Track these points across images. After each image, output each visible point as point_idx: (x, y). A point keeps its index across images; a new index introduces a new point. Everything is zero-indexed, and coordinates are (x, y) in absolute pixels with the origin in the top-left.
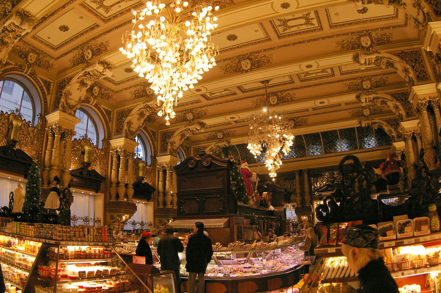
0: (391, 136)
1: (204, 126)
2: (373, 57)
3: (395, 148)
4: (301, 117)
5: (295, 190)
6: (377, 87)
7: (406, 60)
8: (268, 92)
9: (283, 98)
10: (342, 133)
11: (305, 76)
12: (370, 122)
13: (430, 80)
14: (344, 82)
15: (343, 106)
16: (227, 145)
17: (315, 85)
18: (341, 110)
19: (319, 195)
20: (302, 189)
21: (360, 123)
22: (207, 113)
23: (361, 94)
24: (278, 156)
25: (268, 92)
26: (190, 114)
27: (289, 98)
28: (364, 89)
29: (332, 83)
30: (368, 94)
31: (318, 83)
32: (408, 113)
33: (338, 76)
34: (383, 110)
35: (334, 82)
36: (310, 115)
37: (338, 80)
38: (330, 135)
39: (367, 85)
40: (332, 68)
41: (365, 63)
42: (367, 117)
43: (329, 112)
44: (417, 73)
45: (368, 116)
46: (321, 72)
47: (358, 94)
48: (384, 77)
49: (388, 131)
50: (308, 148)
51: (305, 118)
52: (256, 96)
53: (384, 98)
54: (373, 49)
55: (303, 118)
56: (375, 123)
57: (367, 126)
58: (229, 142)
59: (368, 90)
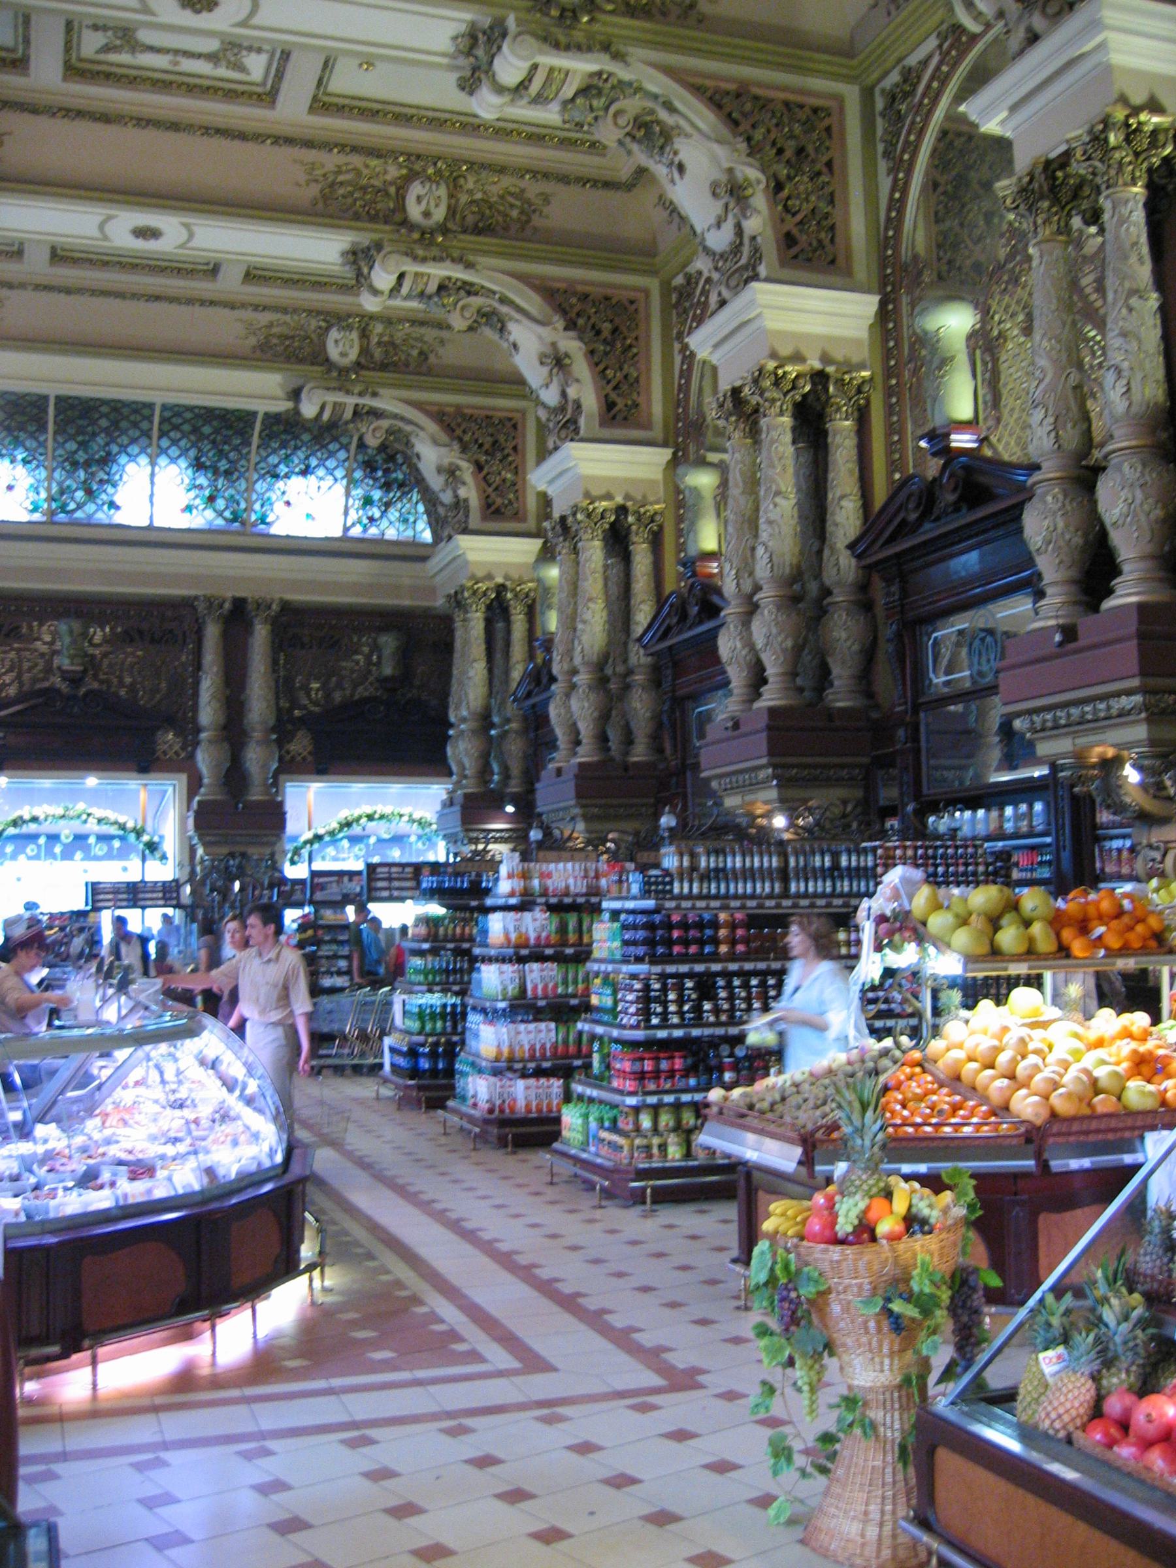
1: (954, 197)
2: (581, 66)
6: (477, 231)
7: (749, 139)
11: (107, 49)
12: (351, 401)
13: (848, 272)
14: (312, 155)
15: (230, 283)
21: (295, 395)
23: (379, 246)
28: (405, 222)
29: (242, 136)
31: (161, 114)
32: (610, 405)
33: (292, 109)
34: (432, 359)
35: (258, 137)
38: (104, 423)
39: (424, 203)
40: (286, 55)
41: (523, 85)
42: (343, 372)
43: (135, 296)
44: (790, 223)
46: (213, 58)
47: (364, 238)
48: (533, 189)
53: (504, 300)
54: (596, 27)
56: (376, 414)
57: (326, 416)
59: (426, 236)
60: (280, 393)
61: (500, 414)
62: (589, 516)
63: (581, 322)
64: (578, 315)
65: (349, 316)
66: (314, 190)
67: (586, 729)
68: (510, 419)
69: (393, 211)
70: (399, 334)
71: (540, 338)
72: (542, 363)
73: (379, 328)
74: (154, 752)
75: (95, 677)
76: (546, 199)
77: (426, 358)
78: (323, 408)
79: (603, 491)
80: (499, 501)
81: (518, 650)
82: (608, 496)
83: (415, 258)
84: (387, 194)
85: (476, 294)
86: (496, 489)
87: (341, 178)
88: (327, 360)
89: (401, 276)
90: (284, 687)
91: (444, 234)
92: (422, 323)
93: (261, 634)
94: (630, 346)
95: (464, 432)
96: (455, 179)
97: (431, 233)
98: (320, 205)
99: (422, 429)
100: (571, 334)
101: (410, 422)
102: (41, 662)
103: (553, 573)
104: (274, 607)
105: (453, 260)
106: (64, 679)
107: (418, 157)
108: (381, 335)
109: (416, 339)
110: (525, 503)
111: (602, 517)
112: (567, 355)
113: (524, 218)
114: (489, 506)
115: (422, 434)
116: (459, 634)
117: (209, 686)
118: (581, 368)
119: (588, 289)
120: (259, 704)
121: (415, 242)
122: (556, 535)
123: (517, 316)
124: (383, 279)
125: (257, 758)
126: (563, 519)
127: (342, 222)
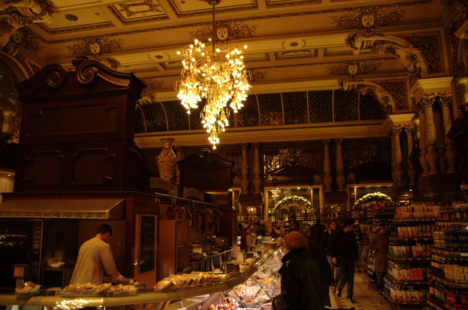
0: (386, 106)
3: (391, 122)
4: (257, 68)
5: (240, 170)
6: (383, 25)
8: (216, 19)
9: (237, 32)
10: (312, 97)
12: (356, 83)
16: (150, 101)
17: (288, 15)
18: (317, 64)
19: (273, 180)
20: (250, 169)
21: (341, 84)
22: (121, 46)
23: (355, 35)
24: (223, 112)
25: (216, 19)
26: (96, 45)
27: (246, 32)
28: (362, 27)
30: (367, 35)
34: (378, 69)
36: (271, 67)
37: (326, 9)
39: (367, 21)
42: (353, 76)
43: (298, 65)
45: (355, 75)
47: (351, 34)
49: (383, 98)
50: (262, 114)
51: (263, 71)
52: (196, 24)
53: (394, 43)
55: (259, 70)
56: (364, 86)
57: (350, 89)
58: (152, 98)
60: (338, 84)
61: (399, 81)
62: (427, 101)
63: (419, 45)
64: (417, 43)
65: (353, 61)
66: (336, 24)
67: (432, 165)
68: (402, 82)
69: (358, 25)
70: (368, 64)
71: (406, 52)
72: (407, 59)
73: (362, 63)
74: (313, 180)
75: (298, 162)
76: (404, 12)
77: (376, 69)
78: (349, 86)
79: (430, 93)
80: (401, 105)
81: (410, 146)
82: (433, 94)
83: (366, 36)
84: (356, 20)
85: (385, 43)
86: (399, 101)
87: (343, 19)
88: (349, 74)
89: (363, 42)
90: (346, 162)
91: (374, 28)
92: (373, 60)
93: (339, 147)
94: (435, 49)
95: (389, 87)
96: (375, 12)
97: (370, 29)
98: (338, 28)
99: (377, 88)
100: (416, 49)
101: (373, 87)
102: (285, 159)
103: (418, 121)
104: (329, 141)
105: (377, 35)
106: (290, 163)
107: (363, 7)
108: (363, 65)
109: (372, 64)
110: (408, 104)
111: (431, 100)
112: (415, 55)
113: (397, 19)
114: (398, 106)
115: (377, 89)
116: (393, 142)
117: (326, 162)
118: (420, 58)
119: (419, 35)
120: (340, 166)
121: (366, 32)
122: (418, 109)
123: (398, 47)
124: (358, 44)
125: (340, 179)
126: (419, 103)
127: (344, 31)
